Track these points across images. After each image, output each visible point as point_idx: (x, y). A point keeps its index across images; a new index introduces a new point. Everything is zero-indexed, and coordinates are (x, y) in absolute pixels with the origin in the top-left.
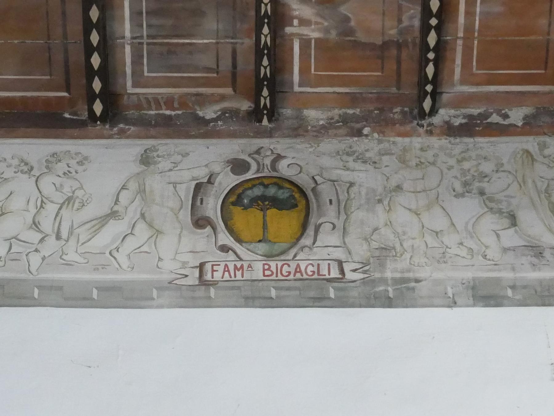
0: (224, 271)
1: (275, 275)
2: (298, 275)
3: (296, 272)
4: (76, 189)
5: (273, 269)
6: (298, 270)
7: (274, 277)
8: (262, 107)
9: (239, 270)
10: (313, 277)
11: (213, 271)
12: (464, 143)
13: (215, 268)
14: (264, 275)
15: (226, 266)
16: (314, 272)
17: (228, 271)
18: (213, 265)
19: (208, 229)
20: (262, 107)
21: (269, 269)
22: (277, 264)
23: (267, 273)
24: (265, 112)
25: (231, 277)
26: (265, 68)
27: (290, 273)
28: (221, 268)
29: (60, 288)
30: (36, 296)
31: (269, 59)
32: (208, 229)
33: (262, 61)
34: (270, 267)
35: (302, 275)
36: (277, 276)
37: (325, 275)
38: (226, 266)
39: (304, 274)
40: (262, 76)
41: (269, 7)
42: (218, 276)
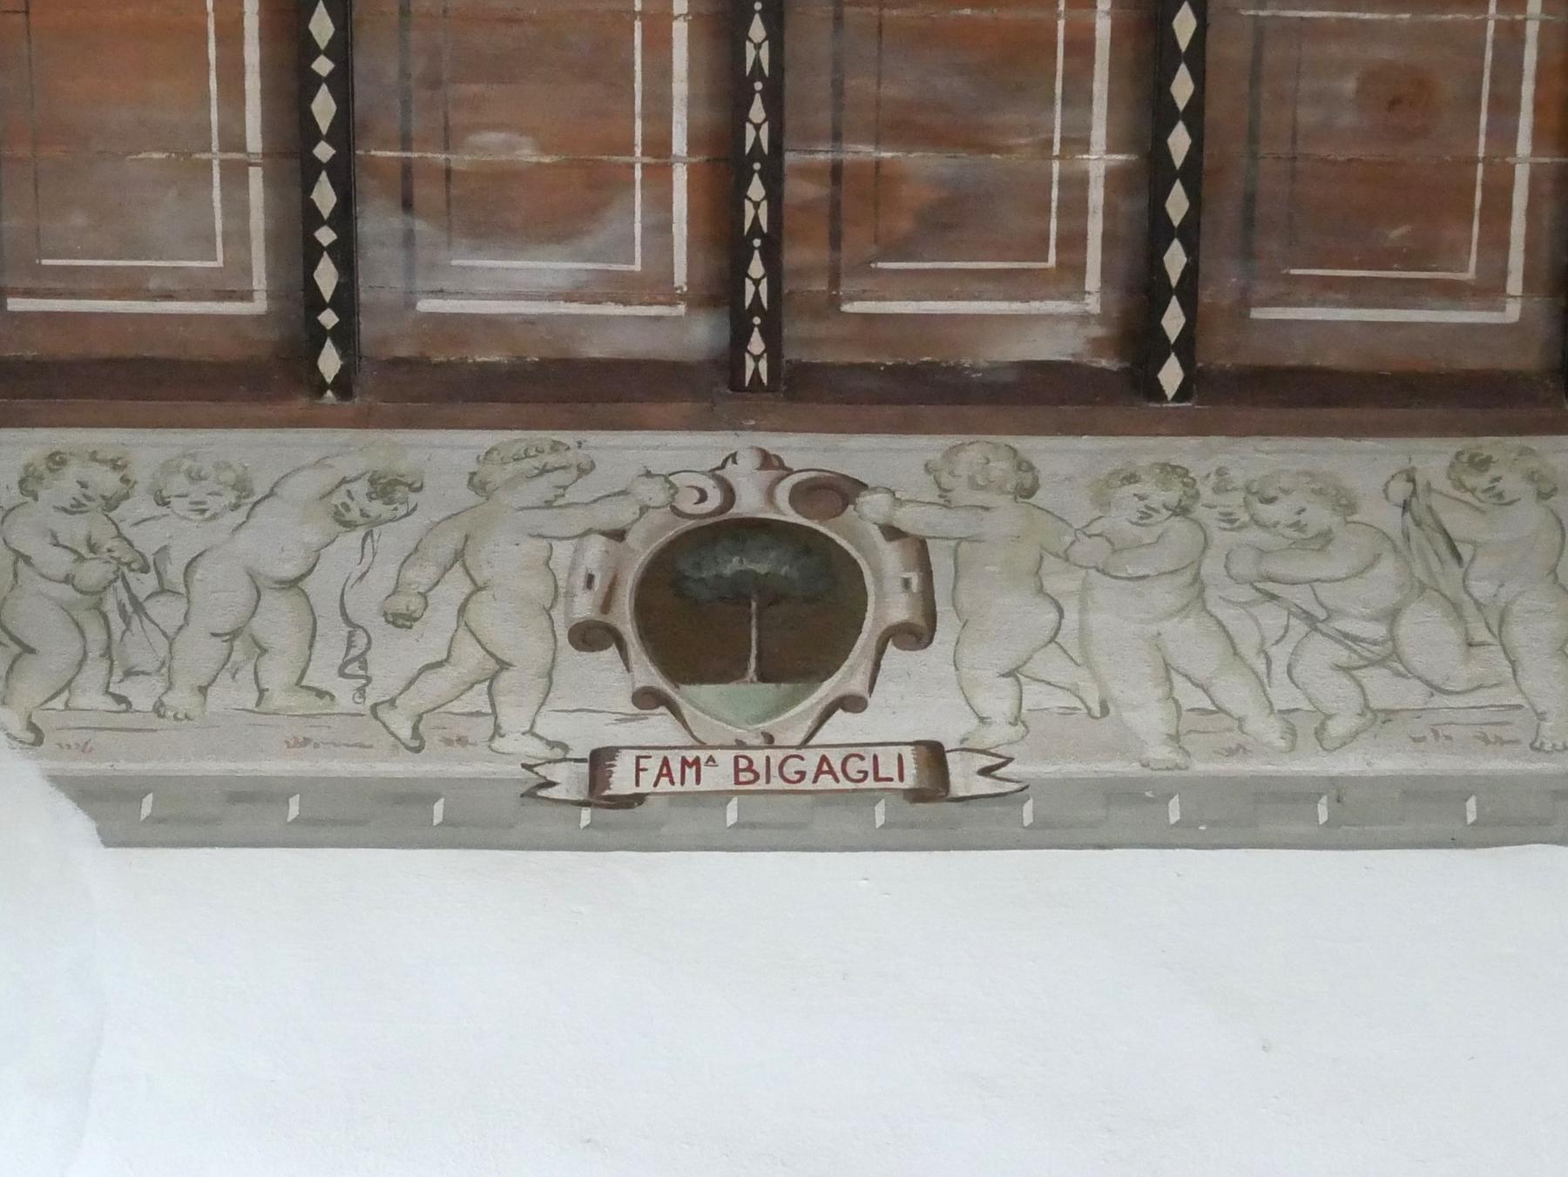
0: (660, 775)
2: (826, 782)
3: (819, 772)
5: (759, 766)
6: (825, 768)
7: (761, 785)
8: (747, 150)
9: (690, 766)
10: (799, 786)
14: (737, 782)
15: (666, 762)
17: (669, 774)
18: (638, 758)
19: (612, 653)
20: (747, 150)
22: (768, 759)
23: (744, 777)
24: (757, 242)
26: (757, 359)
27: (802, 774)
28: (653, 765)
31: (767, 107)
32: (612, 653)
33: (748, 340)
35: (837, 780)
37: (891, 780)
38: (666, 762)
39: (840, 775)
40: (748, 302)
41: (763, 366)
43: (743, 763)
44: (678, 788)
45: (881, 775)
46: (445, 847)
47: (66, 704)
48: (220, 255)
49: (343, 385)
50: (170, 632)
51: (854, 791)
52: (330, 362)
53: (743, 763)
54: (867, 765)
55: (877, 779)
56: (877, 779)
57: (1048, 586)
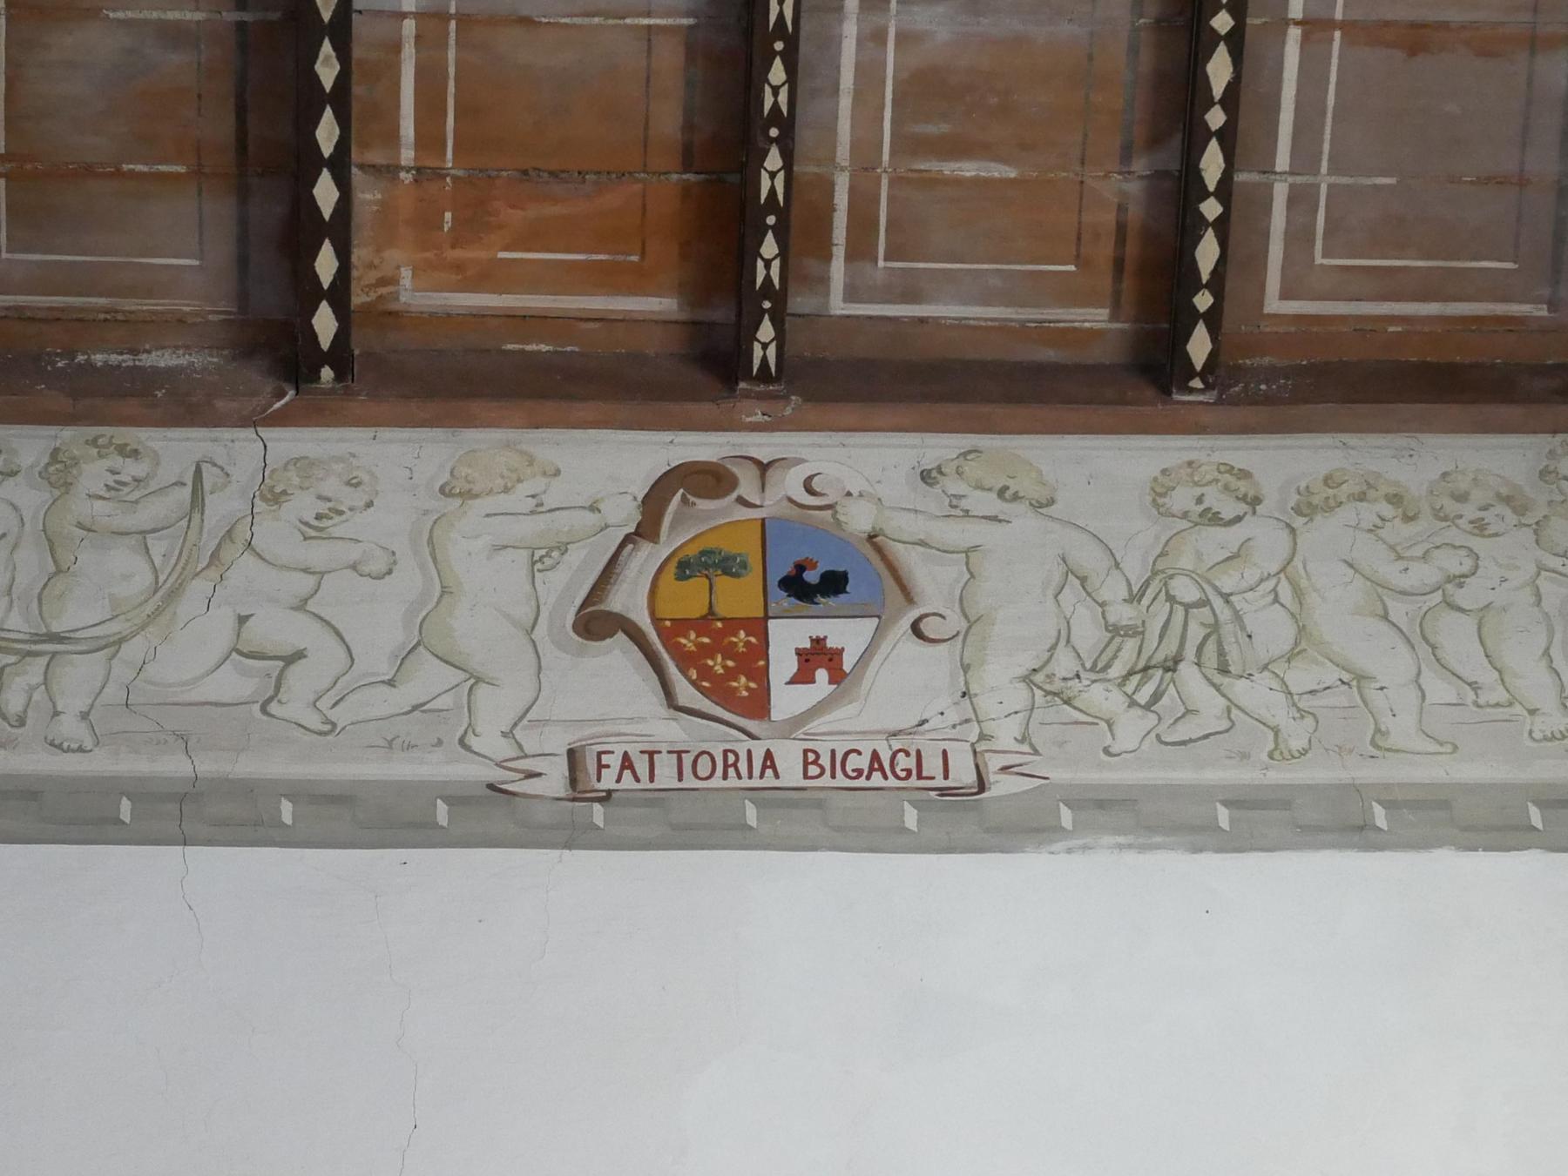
0: (623, 768)
1: (828, 772)
3: (871, 769)
4: (219, 545)
7: (826, 780)
8: (766, 112)
11: (601, 766)
12: (522, 453)
13: (605, 759)
14: (806, 776)
16: (909, 772)
17: (631, 767)
20: (766, 112)
21: (815, 762)
23: (813, 770)
25: (637, 780)
29: (1445, 805)
30: (287, 818)
34: (818, 756)
35: (886, 777)
36: (833, 776)
42: (608, 781)
43: (811, 757)
44: (645, 783)
45: (925, 774)
46: (545, 847)
47: (1511, 704)
48: (1326, 262)
49: (340, 356)
50: (311, 606)
51: (898, 789)
52: (1199, 346)
53: (811, 757)
54: (911, 763)
55: (920, 777)
56: (920, 777)
57: (1022, 543)
